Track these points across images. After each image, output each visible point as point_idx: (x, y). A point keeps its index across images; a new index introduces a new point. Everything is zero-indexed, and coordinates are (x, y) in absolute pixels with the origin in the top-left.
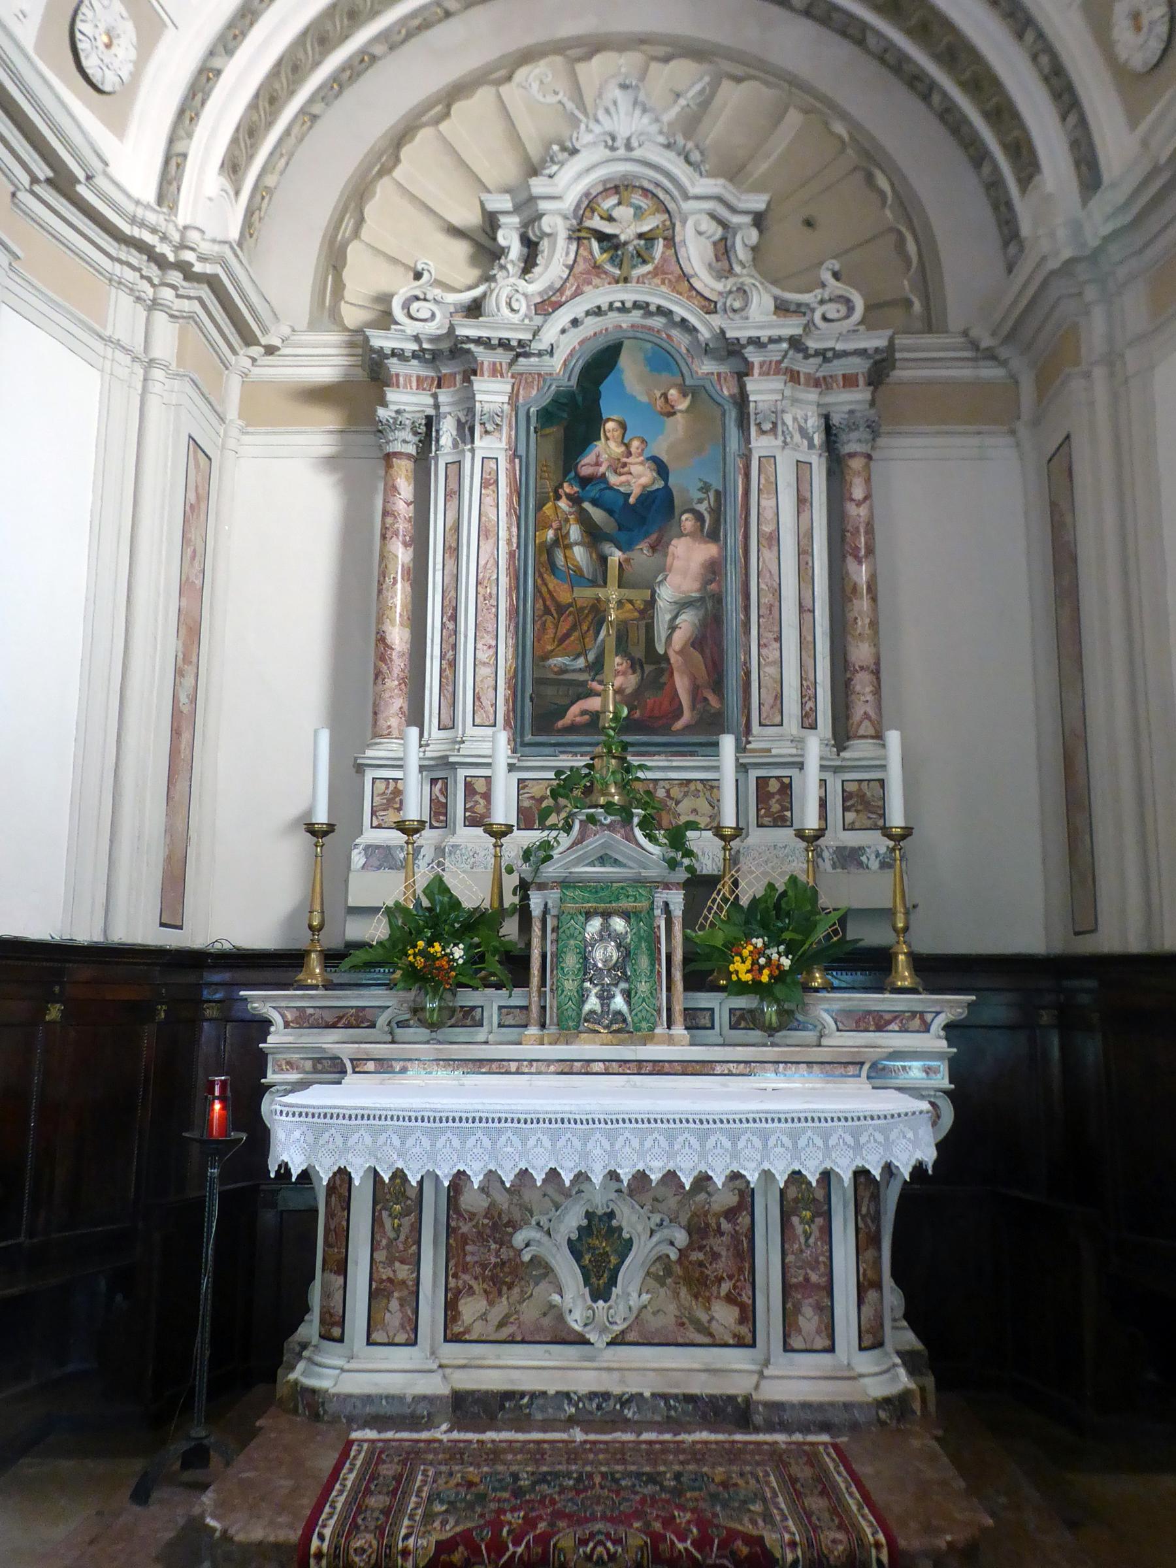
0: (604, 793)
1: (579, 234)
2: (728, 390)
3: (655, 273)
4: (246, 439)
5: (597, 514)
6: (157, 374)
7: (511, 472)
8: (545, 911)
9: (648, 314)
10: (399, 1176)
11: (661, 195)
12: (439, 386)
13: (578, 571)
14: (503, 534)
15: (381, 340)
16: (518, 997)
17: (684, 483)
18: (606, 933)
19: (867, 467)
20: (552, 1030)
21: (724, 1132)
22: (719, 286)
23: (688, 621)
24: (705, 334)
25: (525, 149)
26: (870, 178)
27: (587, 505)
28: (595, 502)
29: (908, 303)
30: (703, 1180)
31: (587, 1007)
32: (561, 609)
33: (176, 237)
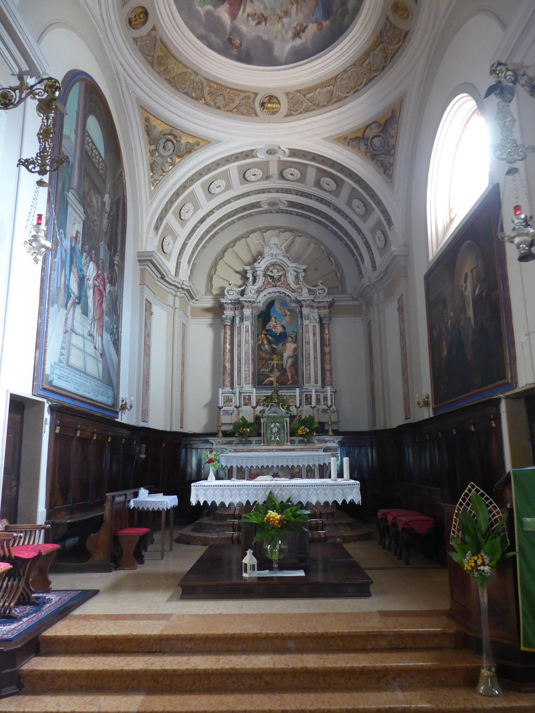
0: (275, 400)
1: (265, 275)
2: (298, 310)
3: (282, 284)
4: (192, 320)
5: (270, 338)
6: (177, 310)
7: (251, 329)
8: (264, 422)
9: (280, 293)
10: (241, 467)
11: (283, 266)
12: (235, 310)
13: (267, 350)
14: (250, 342)
15: (223, 301)
16: (259, 438)
17: (289, 331)
18: (275, 426)
19: (328, 326)
20: (266, 444)
21: (296, 458)
22: (296, 287)
23: (290, 360)
24: (293, 298)
25: (252, 253)
26: (329, 259)
27: (268, 336)
28: (270, 335)
29: (338, 287)
30: (293, 466)
31: (272, 440)
32: (263, 359)
33: (181, 283)
